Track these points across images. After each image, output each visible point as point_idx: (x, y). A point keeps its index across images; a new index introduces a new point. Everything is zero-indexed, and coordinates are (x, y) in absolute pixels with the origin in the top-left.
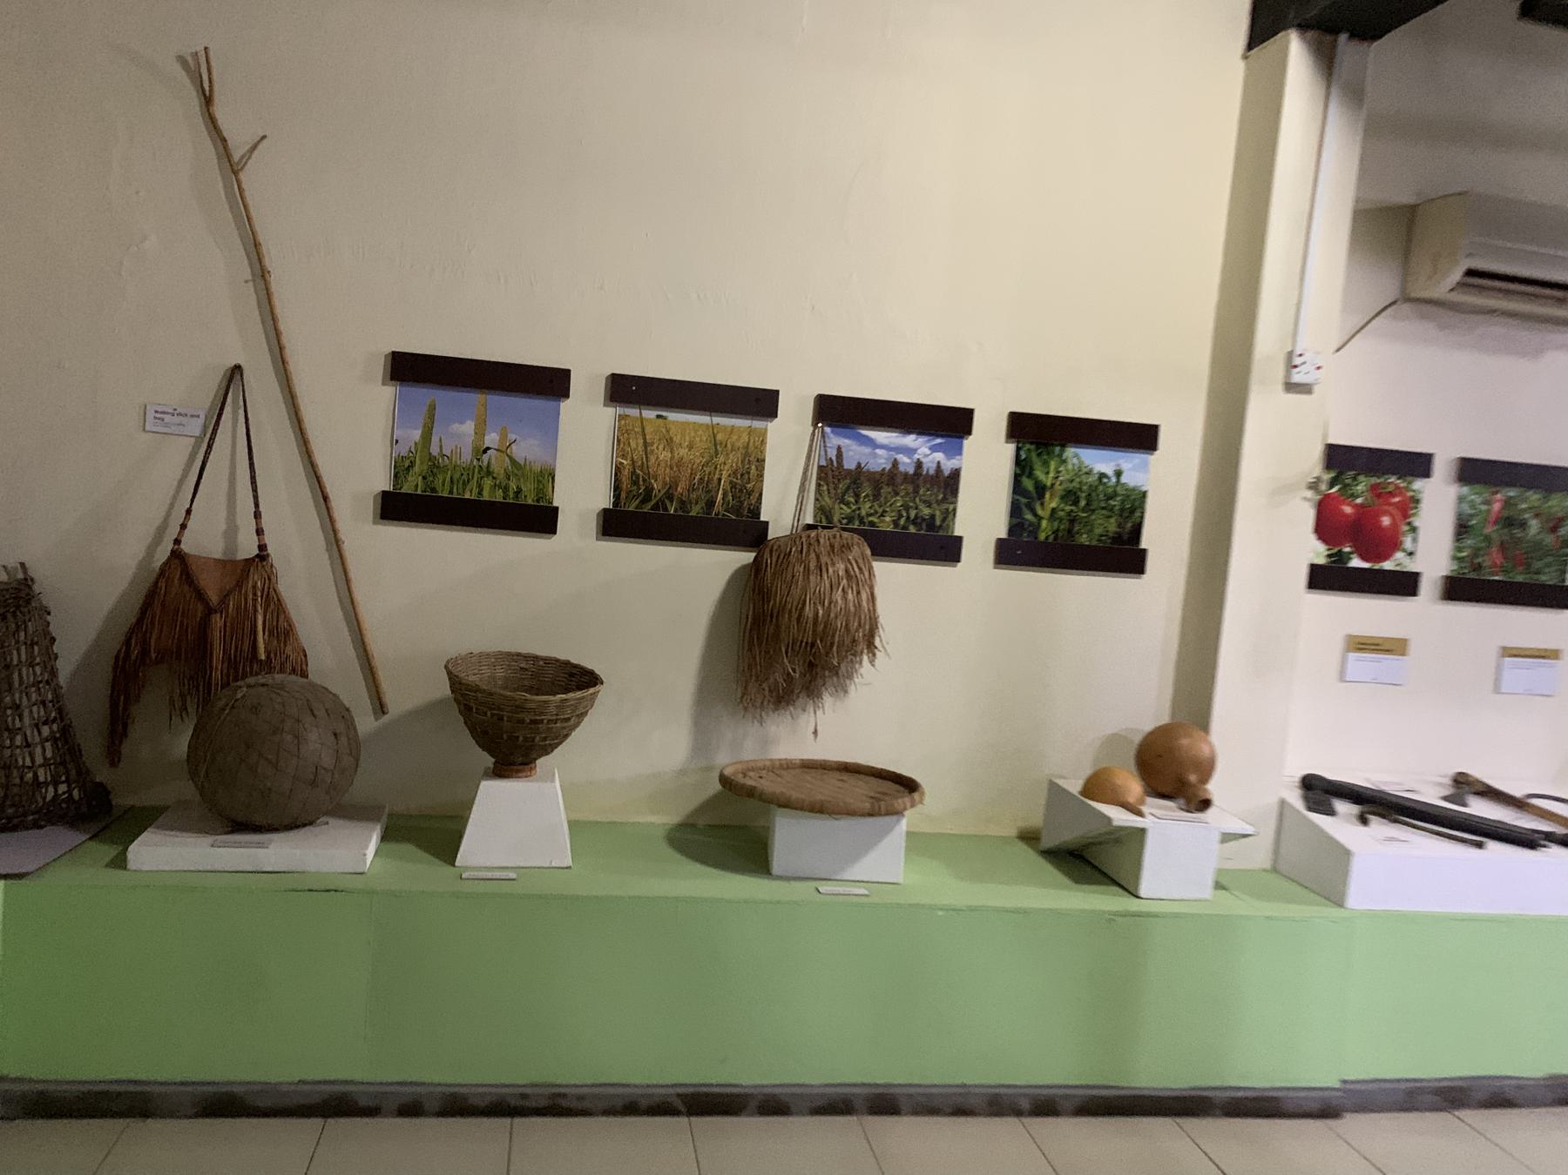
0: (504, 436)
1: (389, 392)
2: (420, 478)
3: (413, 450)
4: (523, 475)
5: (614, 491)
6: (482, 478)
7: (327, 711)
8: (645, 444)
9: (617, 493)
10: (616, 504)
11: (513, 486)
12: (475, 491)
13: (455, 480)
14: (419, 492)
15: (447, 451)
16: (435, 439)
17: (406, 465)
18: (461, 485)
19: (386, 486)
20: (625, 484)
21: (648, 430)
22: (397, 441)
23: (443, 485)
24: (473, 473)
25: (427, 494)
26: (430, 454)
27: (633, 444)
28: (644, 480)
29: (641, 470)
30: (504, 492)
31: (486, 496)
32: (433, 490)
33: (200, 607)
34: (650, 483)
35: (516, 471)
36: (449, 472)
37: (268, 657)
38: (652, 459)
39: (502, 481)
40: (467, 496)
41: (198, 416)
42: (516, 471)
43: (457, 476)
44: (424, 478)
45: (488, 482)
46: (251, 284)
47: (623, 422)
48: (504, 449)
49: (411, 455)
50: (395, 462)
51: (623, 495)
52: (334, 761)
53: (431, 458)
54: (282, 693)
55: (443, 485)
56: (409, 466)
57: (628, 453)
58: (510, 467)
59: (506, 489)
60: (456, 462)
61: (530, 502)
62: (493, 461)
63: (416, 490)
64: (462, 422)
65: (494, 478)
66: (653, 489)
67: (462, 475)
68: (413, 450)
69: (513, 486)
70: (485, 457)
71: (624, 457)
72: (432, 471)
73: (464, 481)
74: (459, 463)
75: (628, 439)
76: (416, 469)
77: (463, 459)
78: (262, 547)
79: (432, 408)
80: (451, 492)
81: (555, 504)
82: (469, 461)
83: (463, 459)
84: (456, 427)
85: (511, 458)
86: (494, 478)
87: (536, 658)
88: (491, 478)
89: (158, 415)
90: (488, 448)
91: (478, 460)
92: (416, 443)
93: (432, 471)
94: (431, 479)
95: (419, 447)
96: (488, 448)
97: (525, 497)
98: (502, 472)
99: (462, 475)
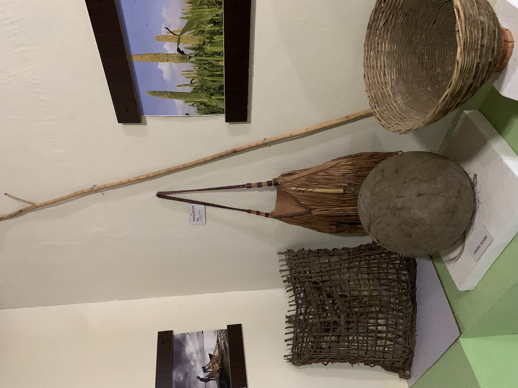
0: (165, 39)
1: (150, 120)
2: (212, 97)
3: (191, 104)
4: (196, 19)
6: (206, 54)
7: (397, 197)
11: (209, 27)
12: (217, 58)
13: (211, 73)
14: (224, 97)
15: (188, 81)
16: (179, 90)
17: (204, 107)
18: (215, 69)
19: (222, 117)
22: (187, 114)
23: (215, 81)
24: (203, 60)
25: (224, 91)
26: (192, 92)
30: (215, 35)
31: (222, 49)
32: (221, 88)
33: (307, 215)
35: (195, 26)
36: (204, 78)
37: (341, 187)
39: (205, 37)
40: (223, 63)
41: (193, 207)
42: (195, 26)
43: (207, 72)
44: (212, 95)
45: (209, 48)
46: (104, 193)
48: (177, 37)
49: (195, 105)
50: (203, 114)
52: (440, 197)
53: (195, 91)
54: (379, 220)
55: (215, 81)
56: (205, 105)
58: (192, 31)
59: (213, 33)
60: (195, 74)
61: (222, 11)
62: (189, 45)
63: (222, 99)
64: (161, 72)
65: (204, 44)
67: (205, 69)
68: (191, 104)
69: (209, 27)
70: (187, 52)
72: (206, 90)
73: (209, 67)
74: (195, 72)
76: (206, 100)
77: (192, 69)
78: (269, 184)
79: (154, 93)
80: (221, 75)
82: (192, 64)
83: (192, 69)
84: (166, 76)
85: (183, 32)
86: (204, 44)
87: (376, 11)
88: (204, 46)
89: (196, 220)
90: (179, 50)
91: (190, 57)
92: (186, 102)
93: (206, 90)
94: (212, 90)
95: (188, 100)
96: (179, 50)
97: (217, 15)
98: (197, 37)
99: (205, 69)
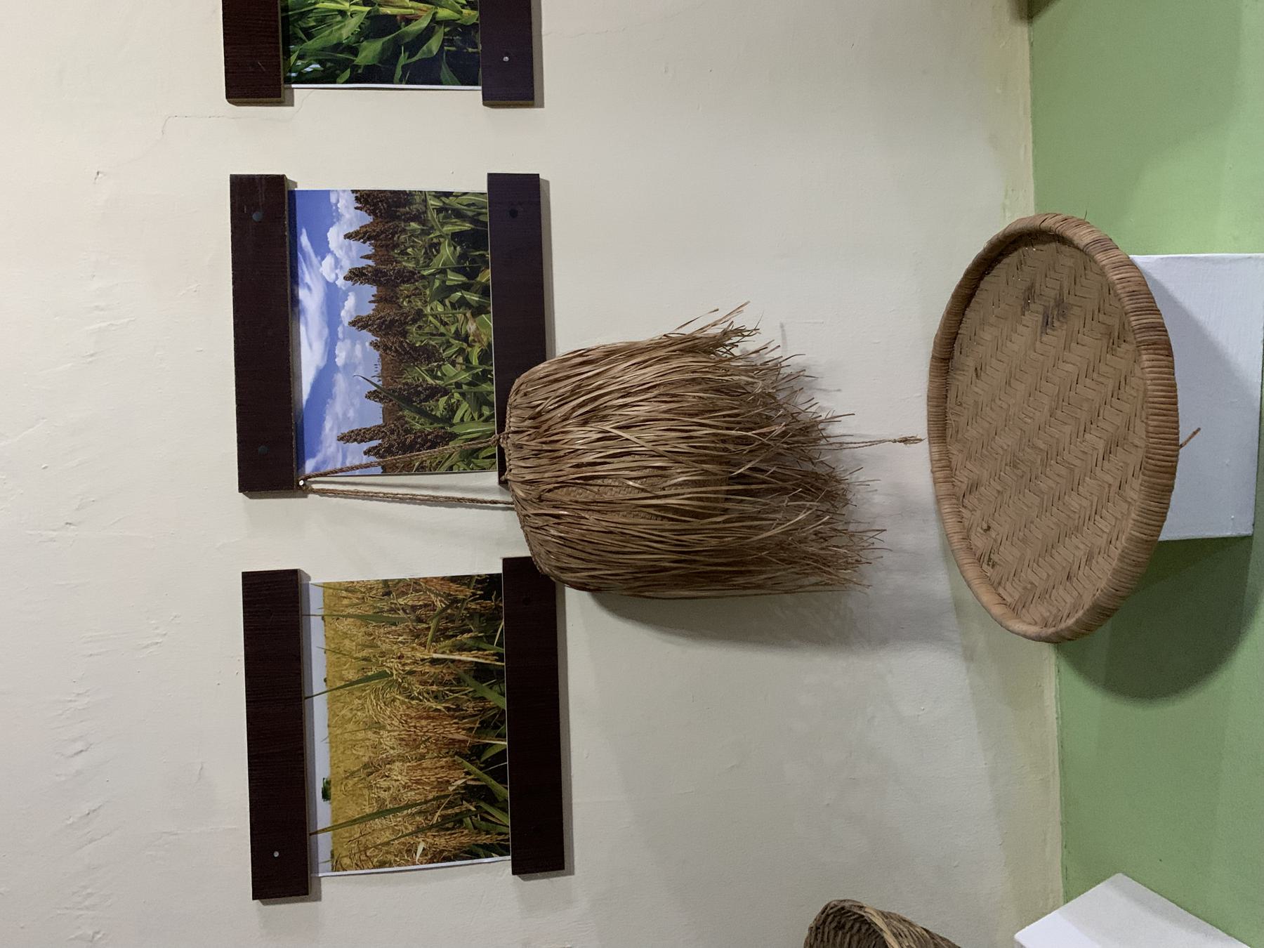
5: (479, 857)
8: (382, 813)
9: (481, 851)
10: (500, 850)
20: (463, 838)
21: (353, 812)
27: (386, 836)
28: (451, 805)
29: (433, 814)
34: (456, 792)
38: (410, 796)
47: (346, 861)
51: (484, 839)
57: (404, 844)
66: (466, 787)
71: (411, 850)
75: (376, 847)
80: (508, 840)
81: (498, 569)
